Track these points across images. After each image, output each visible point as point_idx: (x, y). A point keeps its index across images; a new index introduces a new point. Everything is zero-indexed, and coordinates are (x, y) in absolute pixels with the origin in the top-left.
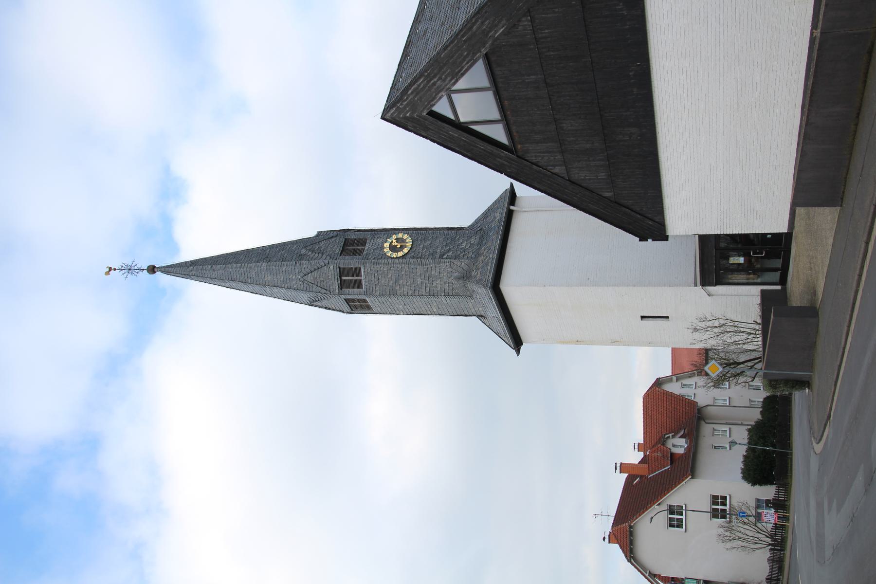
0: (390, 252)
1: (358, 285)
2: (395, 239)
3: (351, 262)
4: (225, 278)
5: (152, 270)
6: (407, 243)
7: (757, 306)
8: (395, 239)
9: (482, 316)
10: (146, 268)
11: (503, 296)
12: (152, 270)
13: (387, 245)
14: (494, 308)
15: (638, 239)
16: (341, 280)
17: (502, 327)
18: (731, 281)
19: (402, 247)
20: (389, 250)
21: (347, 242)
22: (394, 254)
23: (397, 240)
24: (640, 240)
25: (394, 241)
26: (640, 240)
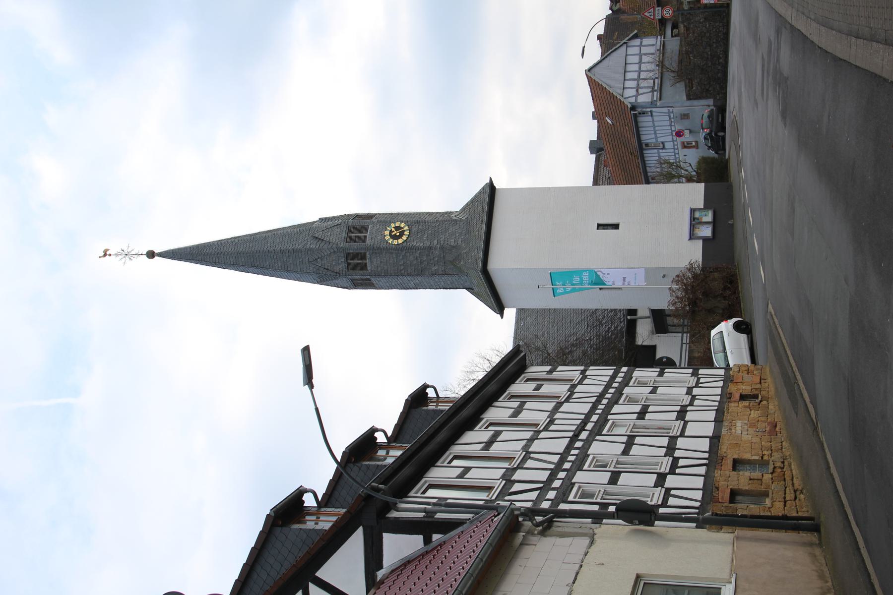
0: (391, 240)
1: (363, 267)
2: (394, 228)
3: (354, 246)
4: (241, 264)
5: (151, 255)
6: (403, 228)
7: (667, 284)
8: (394, 228)
9: (470, 289)
10: (145, 253)
11: (493, 284)
12: (151, 255)
13: (387, 233)
14: (485, 287)
15: (578, 472)
16: (348, 263)
17: (485, 290)
18: (531, 543)
19: (402, 234)
20: (389, 238)
21: (350, 229)
22: (395, 241)
23: (397, 228)
24: (599, 37)
25: (393, 229)
26: (599, 37)
